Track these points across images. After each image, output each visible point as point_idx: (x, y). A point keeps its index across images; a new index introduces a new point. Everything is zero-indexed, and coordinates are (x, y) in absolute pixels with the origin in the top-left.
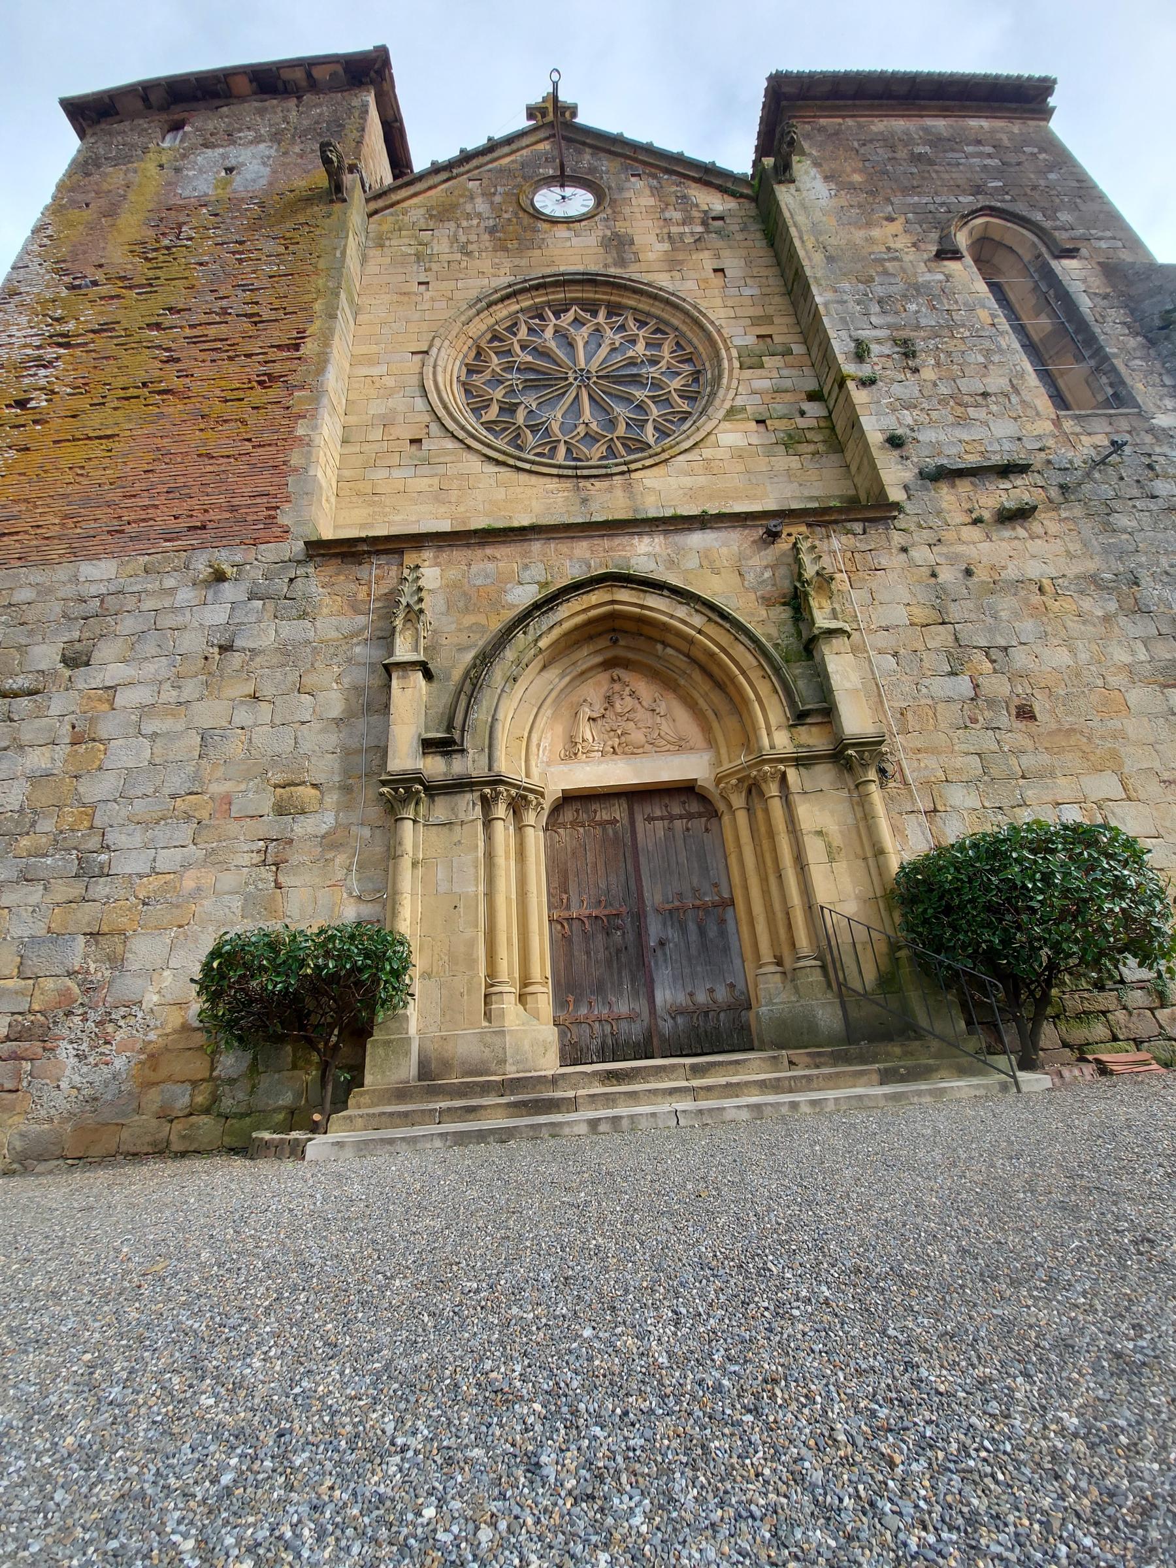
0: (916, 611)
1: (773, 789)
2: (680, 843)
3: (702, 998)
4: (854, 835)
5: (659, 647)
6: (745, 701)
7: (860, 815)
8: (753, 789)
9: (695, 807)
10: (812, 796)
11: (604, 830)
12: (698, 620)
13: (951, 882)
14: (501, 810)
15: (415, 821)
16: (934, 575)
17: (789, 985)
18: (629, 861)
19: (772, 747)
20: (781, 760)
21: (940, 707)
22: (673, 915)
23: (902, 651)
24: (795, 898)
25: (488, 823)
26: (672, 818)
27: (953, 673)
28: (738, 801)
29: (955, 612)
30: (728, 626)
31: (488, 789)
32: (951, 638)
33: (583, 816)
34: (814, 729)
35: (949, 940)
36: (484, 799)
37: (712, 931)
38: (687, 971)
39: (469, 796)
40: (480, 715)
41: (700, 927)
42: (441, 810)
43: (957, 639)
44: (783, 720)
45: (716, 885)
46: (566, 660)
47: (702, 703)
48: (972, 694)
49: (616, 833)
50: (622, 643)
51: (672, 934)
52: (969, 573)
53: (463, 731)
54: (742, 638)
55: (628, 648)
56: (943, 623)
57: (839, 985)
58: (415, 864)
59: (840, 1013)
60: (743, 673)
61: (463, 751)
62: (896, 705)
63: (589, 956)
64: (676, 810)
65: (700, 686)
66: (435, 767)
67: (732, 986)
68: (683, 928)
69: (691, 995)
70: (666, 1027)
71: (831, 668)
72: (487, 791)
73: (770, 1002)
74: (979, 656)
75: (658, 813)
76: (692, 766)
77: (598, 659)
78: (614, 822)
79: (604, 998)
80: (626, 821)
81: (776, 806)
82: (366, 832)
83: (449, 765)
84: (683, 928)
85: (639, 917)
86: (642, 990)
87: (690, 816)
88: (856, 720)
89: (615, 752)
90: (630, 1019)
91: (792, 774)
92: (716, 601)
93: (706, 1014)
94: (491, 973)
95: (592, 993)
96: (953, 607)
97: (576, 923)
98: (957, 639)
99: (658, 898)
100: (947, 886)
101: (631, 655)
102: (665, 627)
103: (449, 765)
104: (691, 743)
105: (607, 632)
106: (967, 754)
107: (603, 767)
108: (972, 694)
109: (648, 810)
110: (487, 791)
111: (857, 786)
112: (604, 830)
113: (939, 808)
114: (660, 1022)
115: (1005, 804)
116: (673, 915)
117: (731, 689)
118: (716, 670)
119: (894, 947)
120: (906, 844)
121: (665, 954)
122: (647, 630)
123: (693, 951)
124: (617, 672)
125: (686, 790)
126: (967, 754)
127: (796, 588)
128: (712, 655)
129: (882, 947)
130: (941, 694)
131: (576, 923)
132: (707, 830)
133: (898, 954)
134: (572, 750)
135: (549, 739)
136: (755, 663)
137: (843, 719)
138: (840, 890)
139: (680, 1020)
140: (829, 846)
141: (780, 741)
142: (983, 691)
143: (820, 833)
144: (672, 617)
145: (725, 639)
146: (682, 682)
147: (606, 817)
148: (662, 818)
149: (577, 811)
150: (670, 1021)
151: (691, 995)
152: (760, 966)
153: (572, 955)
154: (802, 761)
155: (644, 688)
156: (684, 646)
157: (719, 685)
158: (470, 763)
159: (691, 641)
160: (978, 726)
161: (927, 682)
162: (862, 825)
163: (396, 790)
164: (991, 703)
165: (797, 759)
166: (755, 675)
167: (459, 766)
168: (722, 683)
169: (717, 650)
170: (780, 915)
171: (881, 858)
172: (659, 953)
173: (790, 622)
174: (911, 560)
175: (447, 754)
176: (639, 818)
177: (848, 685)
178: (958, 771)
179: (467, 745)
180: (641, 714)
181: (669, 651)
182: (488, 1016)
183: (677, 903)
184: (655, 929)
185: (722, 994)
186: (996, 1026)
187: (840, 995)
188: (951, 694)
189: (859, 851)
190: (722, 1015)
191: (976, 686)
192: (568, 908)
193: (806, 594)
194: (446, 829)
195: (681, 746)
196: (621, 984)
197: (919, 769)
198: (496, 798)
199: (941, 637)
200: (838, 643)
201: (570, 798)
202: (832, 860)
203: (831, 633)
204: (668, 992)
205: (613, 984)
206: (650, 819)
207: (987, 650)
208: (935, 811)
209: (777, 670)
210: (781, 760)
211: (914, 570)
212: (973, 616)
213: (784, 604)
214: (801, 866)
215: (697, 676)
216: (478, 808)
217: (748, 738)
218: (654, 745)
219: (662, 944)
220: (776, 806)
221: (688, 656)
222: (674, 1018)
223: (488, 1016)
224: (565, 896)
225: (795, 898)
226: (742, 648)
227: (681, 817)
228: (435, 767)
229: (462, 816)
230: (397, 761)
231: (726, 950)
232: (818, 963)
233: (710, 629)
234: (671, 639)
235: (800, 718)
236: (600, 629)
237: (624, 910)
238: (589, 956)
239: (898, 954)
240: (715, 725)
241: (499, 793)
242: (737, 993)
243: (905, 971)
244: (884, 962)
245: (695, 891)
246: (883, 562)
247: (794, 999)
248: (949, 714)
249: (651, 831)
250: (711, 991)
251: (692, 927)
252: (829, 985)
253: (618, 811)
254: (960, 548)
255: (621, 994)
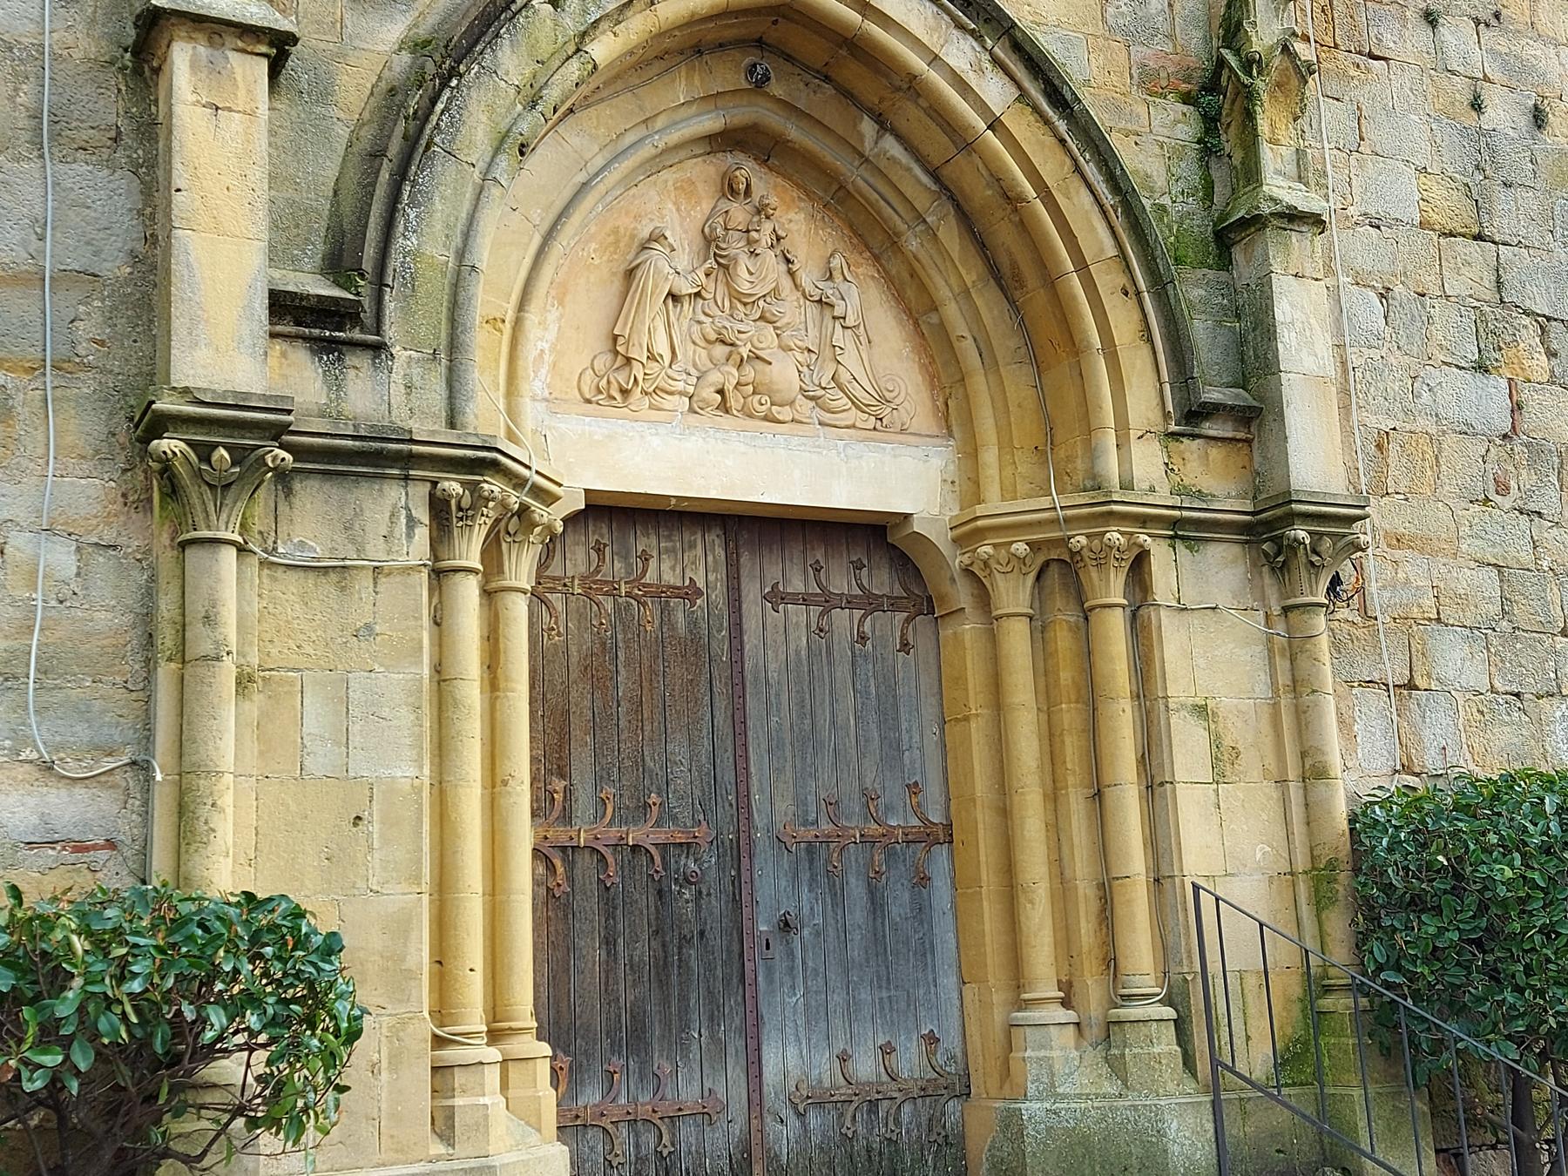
0: (1437, 192)
1: (1113, 588)
2: (843, 671)
3: (866, 1067)
4: (1265, 726)
5: (868, 127)
6: (1073, 345)
7: (1283, 679)
8: (1060, 570)
9: (882, 581)
10: (1195, 619)
11: (665, 610)
12: (995, 91)
13: (1507, 883)
14: (469, 550)
15: (242, 550)
16: (1477, 106)
17: (1093, 1056)
18: (721, 704)
19: (1127, 486)
20: (1144, 521)
21: (1451, 440)
22: (814, 858)
23: (1398, 289)
24: (1135, 861)
25: (440, 575)
26: (828, 602)
27: (1481, 368)
28: (1013, 595)
29: (1508, 214)
30: (1062, 126)
31: (459, 481)
32: (1489, 279)
33: (615, 568)
34: (1215, 452)
35: (1480, 1000)
36: (440, 508)
37: (899, 902)
38: (837, 998)
39: (394, 493)
40: (425, 241)
41: (872, 891)
42: (311, 521)
43: (1499, 284)
44: (1155, 415)
45: (914, 789)
46: (625, 102)
47: (952, 312)
48: (1507, 428)
49: (693, 623)
50: (776, 88)
51: (808, 904)
52: (1539, 118)
53: (380, 285)
54: (1091, 170)
55: (788, 107)
56: (1479, 237)
57: (1215, 1063)
58: (244, 682)
59: (1210, 1126)
60: (1082, 266)
61: (378, 349)
62: (1372, 421)
63: (611, 952)
64: (841, 583)
65: (953, 273)
66: (296, 380)
67: (932, 1039)
68: (837, 895)
69: (843, 1058)
70: (783, 1135)
71: (1283, 311)
72: (452, 486)
73: (1051, 1092)
74: (1529, 335)
75: (797, 585)
76: (895, 476)
77: (711, 123)
78: (690, 593)
79: (644, 1064)
80: (719, 595)
81: (1115, 626)
82: (61, 558)
83: (336, 384)
84: (837, 895)
85: (737, 853)
86: (735, 1044)
87: (870, 603)
88: (1315, 459)
89: (724, 407)
90: (705, 1116)
91: (1161, 556)
92: (1047, 42)
93: (873, 1105)
94: (443, 1010)
95: (615, 1048)
96: (1502, 200)
97: (585, 861)
98: (1499, 284)
99: (784, 807)
100: (1502, 891)
101: (794, 132)
102: (912, 86)
103: (336, 384)
104: (903, 416)
105: (740, 43)
106: (1482, 564)
107: (694, 443)
108: (1507, 428)
109: (774, 573)
110: (452, 486)
111: (1286, 610)
112: (665, 610)
113: (1419, 682)
114: (771, 1124)
115: (1530, 687)
116: (814, 858)
117: (1036, 300)
118: (1004, 236)
119: (1316, 986)
120: (1361, 763)
121: (791, 954)
122: (853, 73)
123: (855, 953)
124: (764, 184)
125: (872, 535)
126: (1482, 564)
127: (1221, 63)
128: (1011, 199)
129: (1288, 985)
130: (1452, 413)
131: (585, 861)
132: (905, 646)
133: (1327, 1003)
134: (619, 377)
135: (561, 337)
136: (1111, 251)
137: (1291, 446)
138: (1231, 846)
139: (814, 1120)
140: (1216, 742)
141: (1145, 463)
142: (1528, 421)
143: (1201, 711)
144: (934, 60)
145: (1051, 166)
146: (913, 244)
147: (671, 578)
148: (806, 600)
149: (599, 550)
150: (793, 1121)
151: (843, 1058)
152: (1024, 1005)
153: (571, 948)
154: (1186, 530)
155: (800, 227)
156: (937, 145)
157: (1001, 277)
158: (397, 391)
159: (964, 142)
160: (1507, 503)
161: (1435, 375)
162: (1285, 701)
163: (204, 451)
164: (1536, 451)
165: (1175, 523)
166: (1108, 281)
167: (374, 396)
168: (1016, 270)
169: (1030, 192)
170: (1085, 890)
171: (1320, 787)
172: (777, 949)
173: (1192, 152)
174: (1439, 49)
175: (327, 348)
176: (751, 593)
177: (1309, 364)
178: (1461, 600)
179: (391, 332)
180: (791, 309)
181: (891, 146)
182: (444, 1125)
183: (826, 826)
184: (773, 888)
185: (910, 1061)
186: (1458, 1156)
187: (1215, 1088)
188: (1470, 416)
189: (1271, 761)
190: (907, 1108)
191: (1517, 407)
192: (567, 818)
193: (1248, 96)
194: (328, 585)
195: (879, 420)
196: (685, 1027)
197: (1393, 585)
198: (468, 514)
199: (1469, 270)
200: (1301, 247)
201: (611, 514)
202: (1219, 777)
203: (1293, 217)
204: (792, 1051)
205: (667, 1025)
206: (776, 597)
207: (1544, 323)
208: (1411, 686)
209: (1160, 285)
210: (1144, 521)
211: (1443, 80)
212: (1534, 235)
213: (1187, 99)
214: (1154, 785)
215: (950, 235)
216: (422, 534)
217: (1061, 431)
218: (820, 403)
219: (785, 926)
220: (1115, 626)
221: (934, 175)
222: (800, 1115)
223: (444, 1125)
224: (559, 785)
225: (1135, 861)
226: (1086, 198)
227: (850, 603)
228: (296, 380)
229: (376, 551)
230: (203, 354)
231: (926, 951)
232: (1169, 1012)
233: (1022, 126)
234: (910, 116)
235: (1192, 416)
236: (729, 34)
237: (703, 833)
238: (611, 952)
239: (1327, 1003)
240: (979, 384)
241: (480, 499)
242: (940, 1059)
243: (1343, 1043)
244: (1289, 1019)
245: (868, 797)
246: (1388, 39)
247: (1110, 1088)
248: (1464, 463)
249: (779, 628)
250: (887, 1050)
251: (856, 889)
252: (1188, 1062)
253: (695, 565)
254: (1533, 51)
255: (685, 1050)
